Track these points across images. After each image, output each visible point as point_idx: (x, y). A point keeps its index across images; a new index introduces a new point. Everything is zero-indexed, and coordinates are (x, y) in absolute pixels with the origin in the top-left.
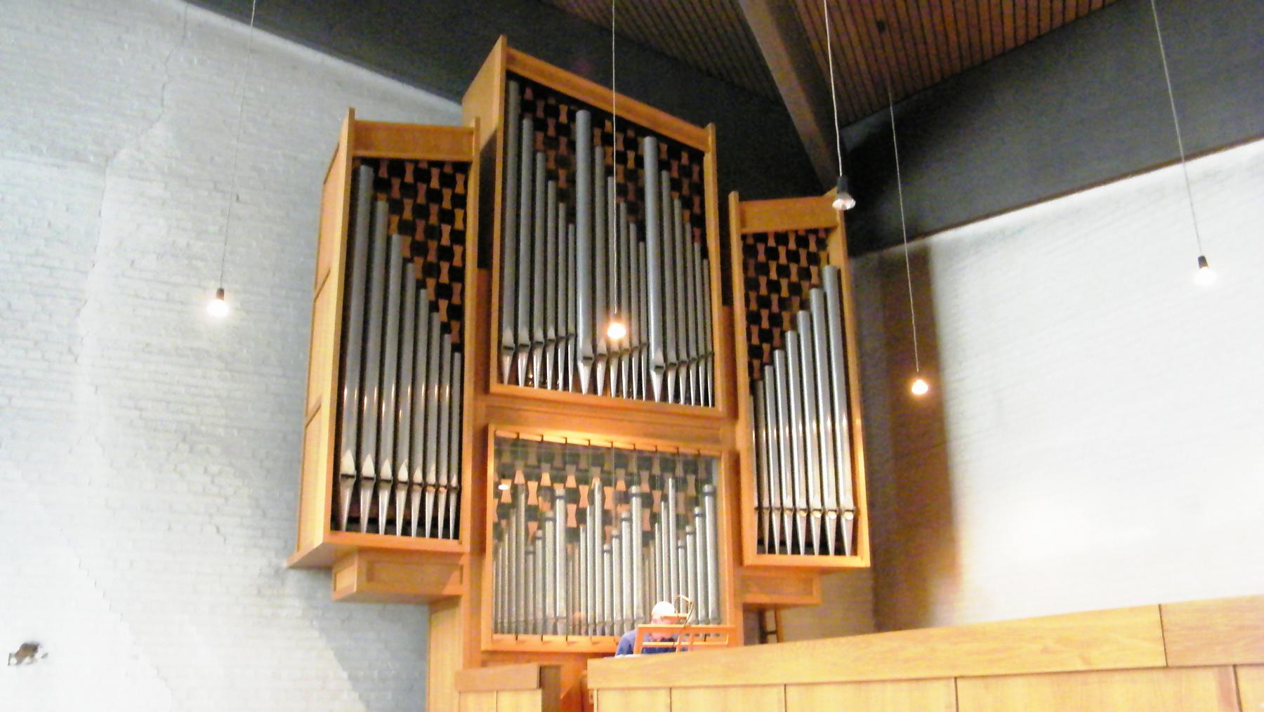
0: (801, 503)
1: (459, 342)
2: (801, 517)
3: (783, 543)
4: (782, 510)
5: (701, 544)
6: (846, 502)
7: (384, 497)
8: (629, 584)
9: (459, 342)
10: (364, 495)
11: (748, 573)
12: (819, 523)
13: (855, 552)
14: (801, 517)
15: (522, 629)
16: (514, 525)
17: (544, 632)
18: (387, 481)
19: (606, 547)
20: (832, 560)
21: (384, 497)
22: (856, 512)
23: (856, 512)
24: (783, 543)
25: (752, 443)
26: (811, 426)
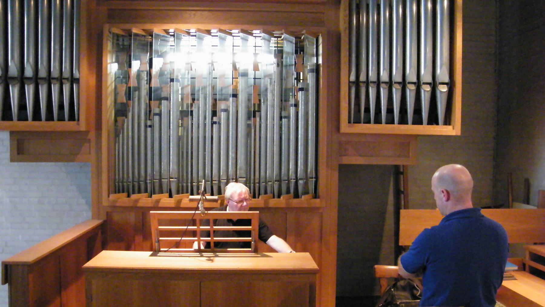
0: (384, 76)
1: (137, 85)
2: (411, 90)
3: (390, 110)
4: (378, 83)
5: (77, 102)
6: (442, 74)
7: (55, 89)
8: (234, 150)
9: (137, 85)
10: (41, 88)
11: (343, 139)
12: (413, 94)
13: (448, 121)
14: (411, 90)
15: (131, 191)
16: (136, 103)
17: (153, 192)
18: (56, 79)
19: (215, 119)
20: (426, 129)
21: (55, 89)
22: (451, 85)
23: (451, 85)
24: (390, 110)
25: (361, 14)
26: (373, 16)
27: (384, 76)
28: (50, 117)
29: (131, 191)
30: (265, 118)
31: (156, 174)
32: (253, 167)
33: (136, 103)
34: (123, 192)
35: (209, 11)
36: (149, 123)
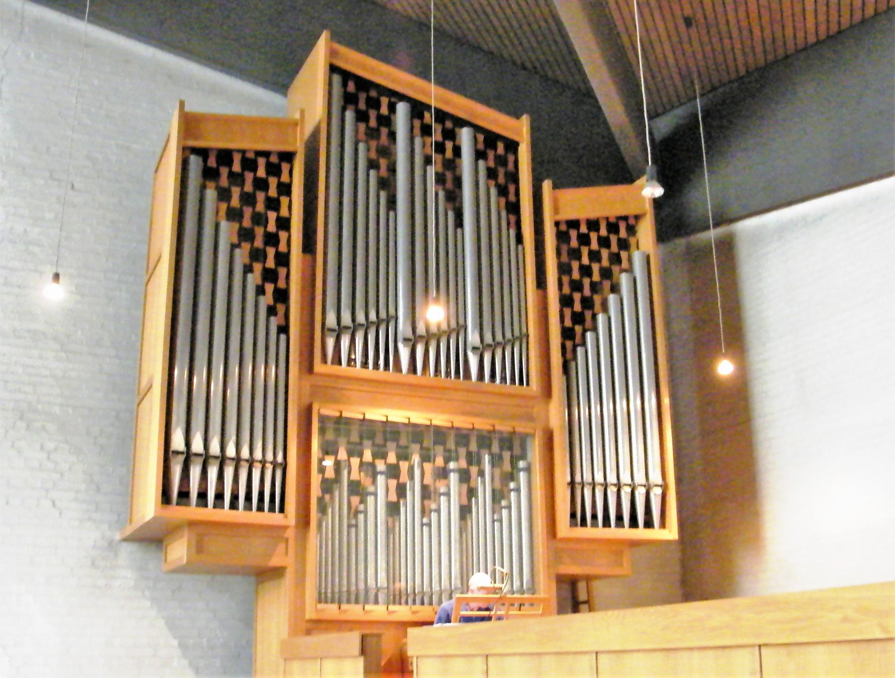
0: (599, 478)
6: (656, 477)
11: (560, 545)
12: (629, 497)
13: (663, 525)
15: (344, 598)
16: (337, 500)
17: (366, 601)
19: (425, 520)
20: (641, 533)
22: (665, 487)
23: (665, 487)
25: (565, 421)
27: (599, 478)
28: (634, 523)
29: (344, 598)
30: (395, 295)
31: (362, 585)
32: (490, 477)
33: (337, 500)
34: (333, 602)
35: (420, 397)
36: (353, 522)
